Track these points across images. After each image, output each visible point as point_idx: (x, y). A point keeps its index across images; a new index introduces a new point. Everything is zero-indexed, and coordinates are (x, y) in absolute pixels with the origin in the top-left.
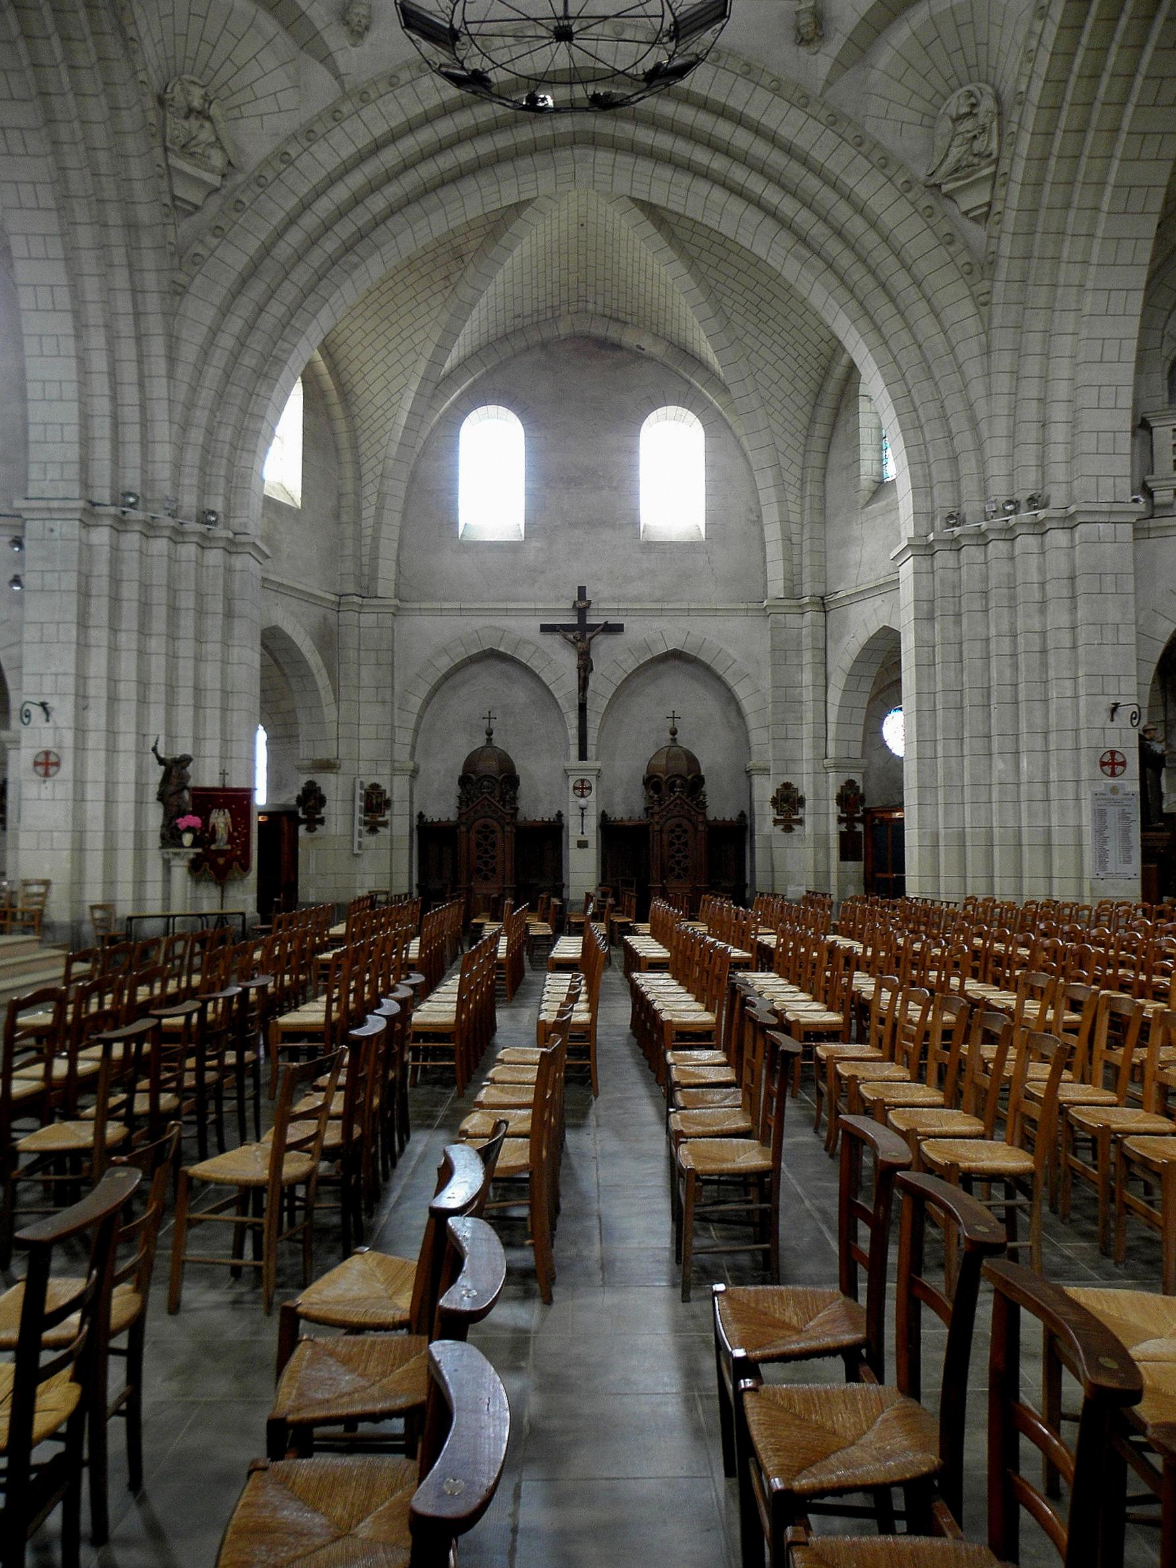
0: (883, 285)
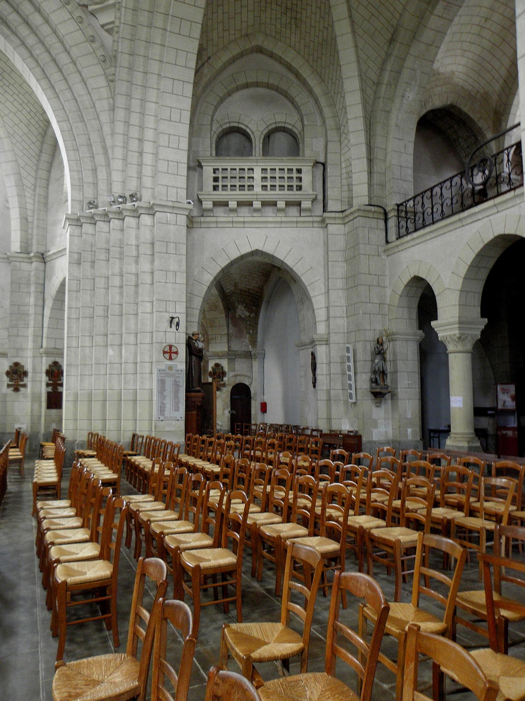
0: (54, 60)
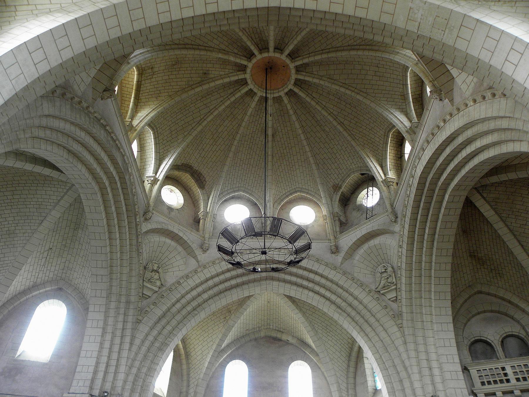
0: (366, 321)
